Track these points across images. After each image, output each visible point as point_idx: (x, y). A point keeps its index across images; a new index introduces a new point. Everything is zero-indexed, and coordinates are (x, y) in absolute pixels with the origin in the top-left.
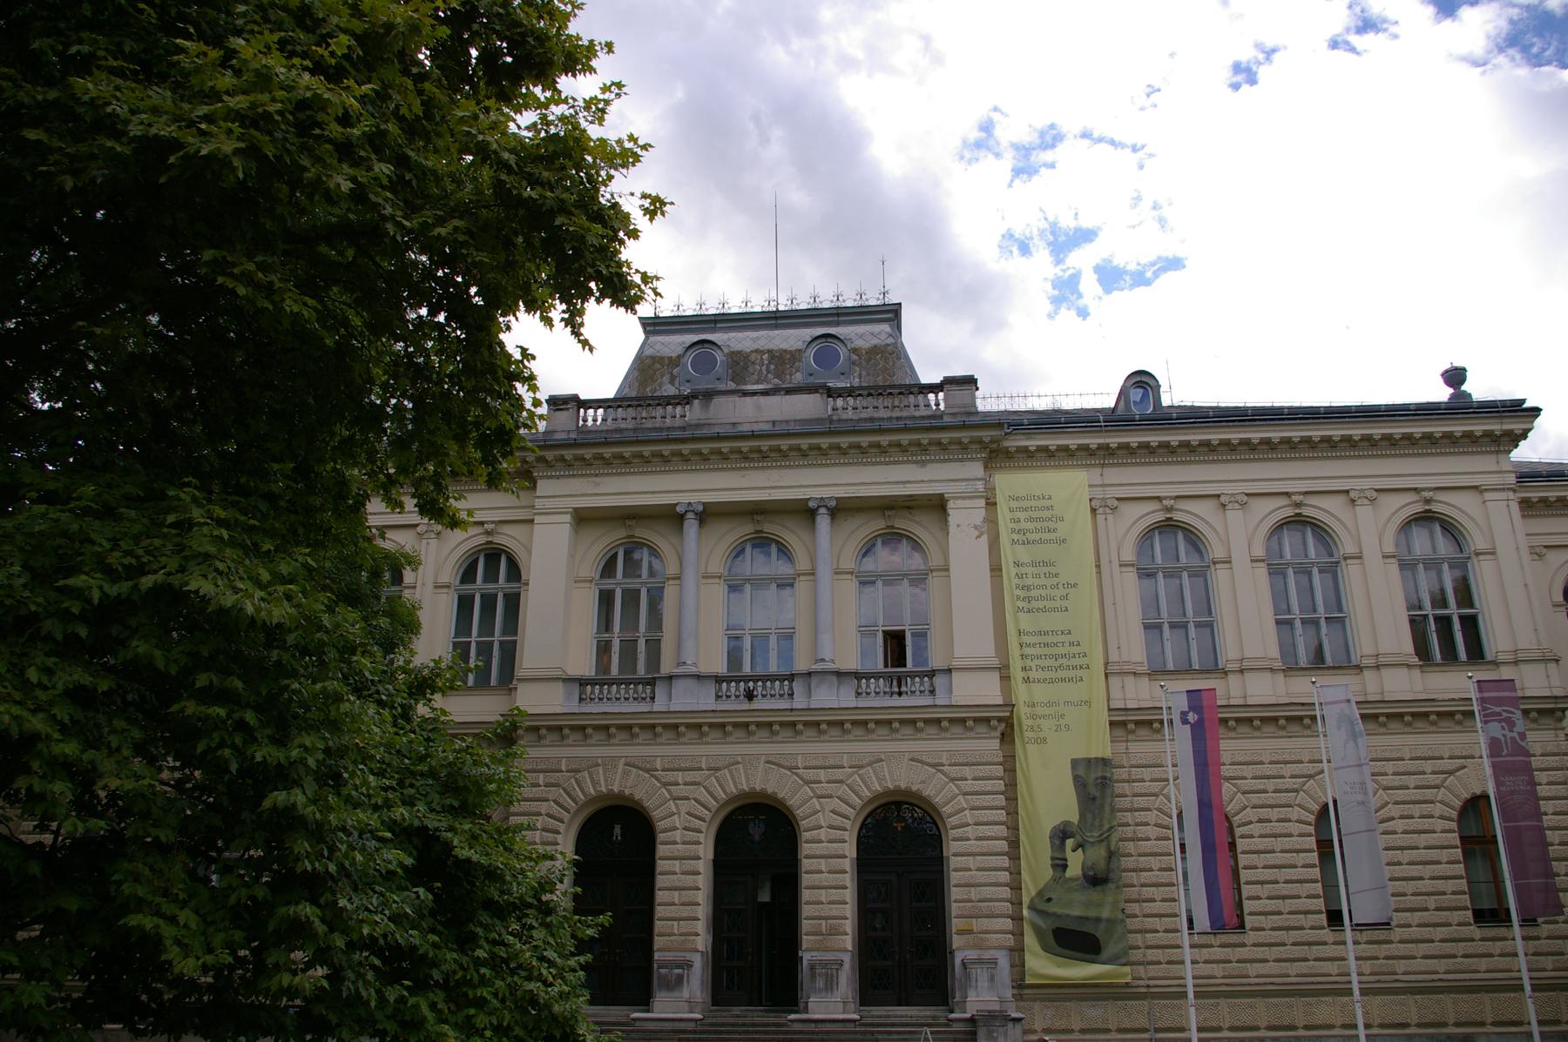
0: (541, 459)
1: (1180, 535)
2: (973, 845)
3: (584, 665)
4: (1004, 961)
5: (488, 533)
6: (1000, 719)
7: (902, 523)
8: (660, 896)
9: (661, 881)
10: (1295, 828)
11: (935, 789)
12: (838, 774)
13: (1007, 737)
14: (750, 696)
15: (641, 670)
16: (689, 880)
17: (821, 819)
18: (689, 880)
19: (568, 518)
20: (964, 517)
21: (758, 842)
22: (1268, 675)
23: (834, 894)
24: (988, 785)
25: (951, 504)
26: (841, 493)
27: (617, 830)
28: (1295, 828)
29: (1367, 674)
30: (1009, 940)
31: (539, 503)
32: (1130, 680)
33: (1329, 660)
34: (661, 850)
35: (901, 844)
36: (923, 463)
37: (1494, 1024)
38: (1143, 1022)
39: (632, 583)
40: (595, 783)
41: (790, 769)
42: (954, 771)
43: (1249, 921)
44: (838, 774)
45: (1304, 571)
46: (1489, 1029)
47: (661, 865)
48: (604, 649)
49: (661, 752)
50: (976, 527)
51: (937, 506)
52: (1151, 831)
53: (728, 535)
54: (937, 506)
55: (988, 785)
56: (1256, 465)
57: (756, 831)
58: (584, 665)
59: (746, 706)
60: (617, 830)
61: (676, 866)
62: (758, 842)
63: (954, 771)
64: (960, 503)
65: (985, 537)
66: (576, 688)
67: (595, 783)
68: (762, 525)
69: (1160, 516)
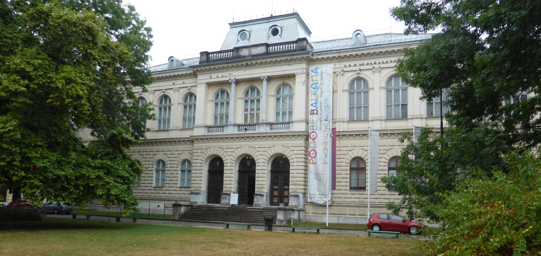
0: (197, 70)
1: (362, 81)
2: (296, 167)
3: (384, 114)
4: (301, 196)
5: (164, 92)
6: (304, 135)
7: (287, 81)
8: (225, 179)
9: (225, 175)
10: (344, 164)
11: (288, 153)
12: (265, 149)
13: (307, 139)
14: (246, 130)
15: (224, 123)
16: (231, 175)
17: (228, 161)
18: (231, 175)
19: (204, 85)
20: (300, 79)
21: (247, 166)
22: (420, 120)
23: (263, 179)
24: (300, 152)
25: (296, 76)
26: (269, 74)
27: (218, 163)
28: (382, 164)
29: (370, 122)
30: (303, 191)
31: (198, 82)
32: (342, 123)
33: (434, 115)
34: (225, 168)
35: (280, 166)
36: (290, 65)
37: (359, 215)
38: (336, 212)
39: (252, 98)
40: (211, 152)
41: (287, 147)
42: (258, 149)
43: (337, 188)
44: (265, 149)
45: (397, 90)
46: (357, 216)
47: (225, 171)
48: (246, 116)
49: (225, 144)
50: (302, 82)
51: (292, 76)
52: (175, 166)
53: (242, 89)
54: (292, 76)
55: (300, 152)
56: (296, 65)
57: (249, 163)
58: (210, 122)
59: (244, 133)
60: (218, 163)
61: (260, 172)
62: (247, 166)
63: (258, 149)
64: (300, 76)
65: (305, 85)
66: (207, 129)
67: (211, 152)
68: (252, 84)
69: (356, 76)
